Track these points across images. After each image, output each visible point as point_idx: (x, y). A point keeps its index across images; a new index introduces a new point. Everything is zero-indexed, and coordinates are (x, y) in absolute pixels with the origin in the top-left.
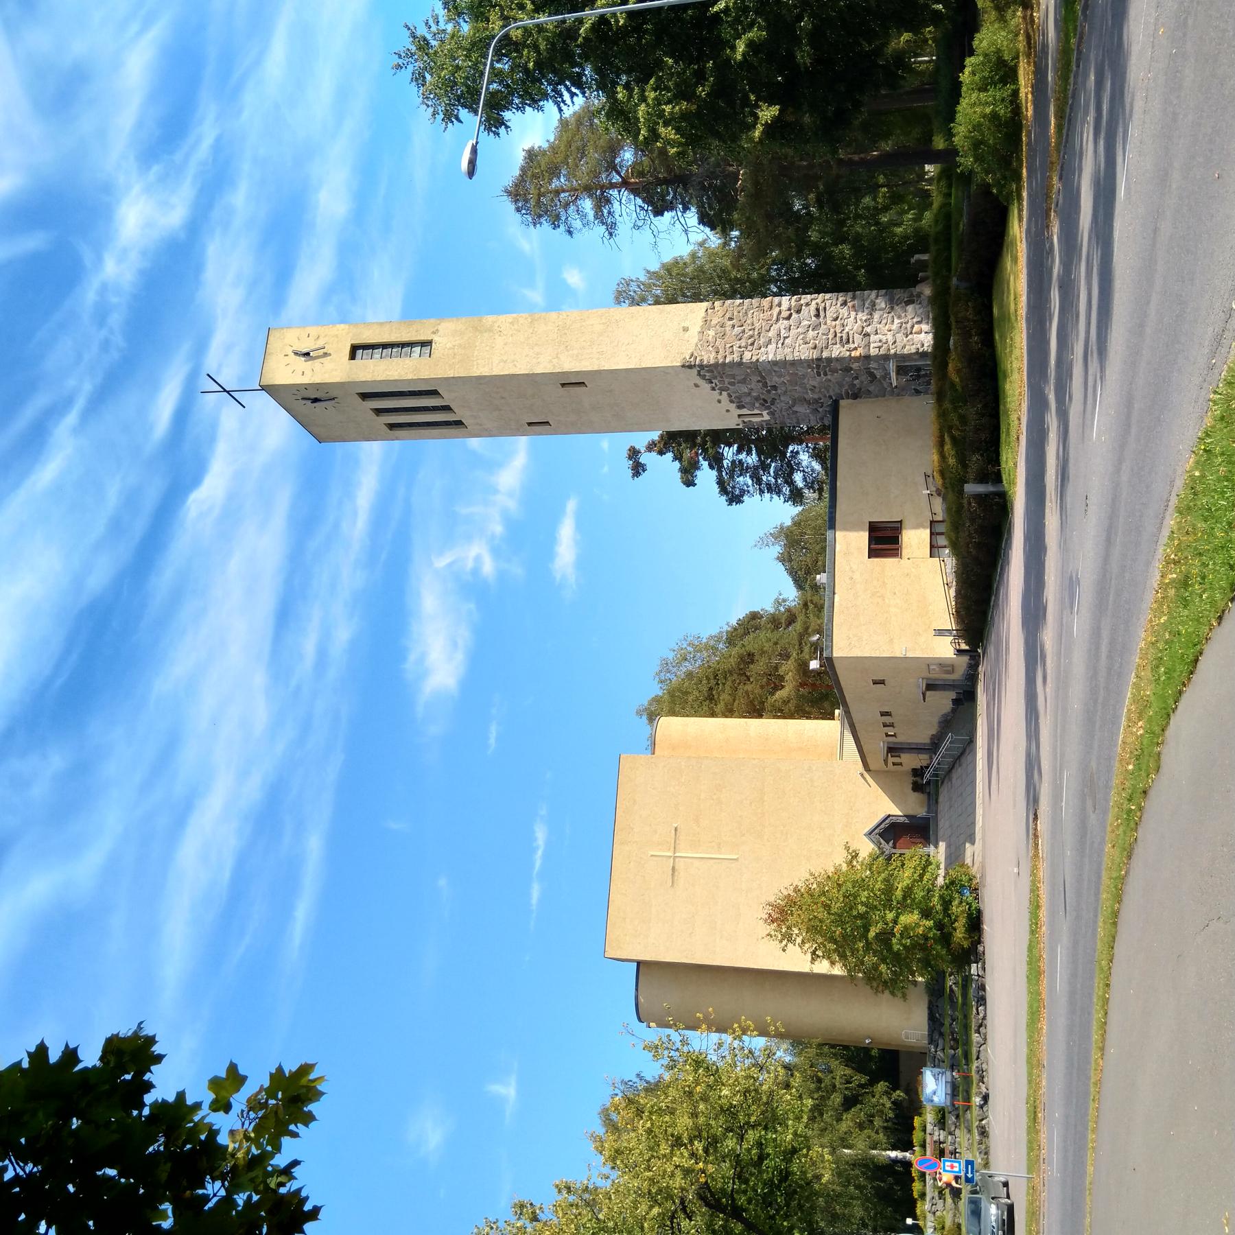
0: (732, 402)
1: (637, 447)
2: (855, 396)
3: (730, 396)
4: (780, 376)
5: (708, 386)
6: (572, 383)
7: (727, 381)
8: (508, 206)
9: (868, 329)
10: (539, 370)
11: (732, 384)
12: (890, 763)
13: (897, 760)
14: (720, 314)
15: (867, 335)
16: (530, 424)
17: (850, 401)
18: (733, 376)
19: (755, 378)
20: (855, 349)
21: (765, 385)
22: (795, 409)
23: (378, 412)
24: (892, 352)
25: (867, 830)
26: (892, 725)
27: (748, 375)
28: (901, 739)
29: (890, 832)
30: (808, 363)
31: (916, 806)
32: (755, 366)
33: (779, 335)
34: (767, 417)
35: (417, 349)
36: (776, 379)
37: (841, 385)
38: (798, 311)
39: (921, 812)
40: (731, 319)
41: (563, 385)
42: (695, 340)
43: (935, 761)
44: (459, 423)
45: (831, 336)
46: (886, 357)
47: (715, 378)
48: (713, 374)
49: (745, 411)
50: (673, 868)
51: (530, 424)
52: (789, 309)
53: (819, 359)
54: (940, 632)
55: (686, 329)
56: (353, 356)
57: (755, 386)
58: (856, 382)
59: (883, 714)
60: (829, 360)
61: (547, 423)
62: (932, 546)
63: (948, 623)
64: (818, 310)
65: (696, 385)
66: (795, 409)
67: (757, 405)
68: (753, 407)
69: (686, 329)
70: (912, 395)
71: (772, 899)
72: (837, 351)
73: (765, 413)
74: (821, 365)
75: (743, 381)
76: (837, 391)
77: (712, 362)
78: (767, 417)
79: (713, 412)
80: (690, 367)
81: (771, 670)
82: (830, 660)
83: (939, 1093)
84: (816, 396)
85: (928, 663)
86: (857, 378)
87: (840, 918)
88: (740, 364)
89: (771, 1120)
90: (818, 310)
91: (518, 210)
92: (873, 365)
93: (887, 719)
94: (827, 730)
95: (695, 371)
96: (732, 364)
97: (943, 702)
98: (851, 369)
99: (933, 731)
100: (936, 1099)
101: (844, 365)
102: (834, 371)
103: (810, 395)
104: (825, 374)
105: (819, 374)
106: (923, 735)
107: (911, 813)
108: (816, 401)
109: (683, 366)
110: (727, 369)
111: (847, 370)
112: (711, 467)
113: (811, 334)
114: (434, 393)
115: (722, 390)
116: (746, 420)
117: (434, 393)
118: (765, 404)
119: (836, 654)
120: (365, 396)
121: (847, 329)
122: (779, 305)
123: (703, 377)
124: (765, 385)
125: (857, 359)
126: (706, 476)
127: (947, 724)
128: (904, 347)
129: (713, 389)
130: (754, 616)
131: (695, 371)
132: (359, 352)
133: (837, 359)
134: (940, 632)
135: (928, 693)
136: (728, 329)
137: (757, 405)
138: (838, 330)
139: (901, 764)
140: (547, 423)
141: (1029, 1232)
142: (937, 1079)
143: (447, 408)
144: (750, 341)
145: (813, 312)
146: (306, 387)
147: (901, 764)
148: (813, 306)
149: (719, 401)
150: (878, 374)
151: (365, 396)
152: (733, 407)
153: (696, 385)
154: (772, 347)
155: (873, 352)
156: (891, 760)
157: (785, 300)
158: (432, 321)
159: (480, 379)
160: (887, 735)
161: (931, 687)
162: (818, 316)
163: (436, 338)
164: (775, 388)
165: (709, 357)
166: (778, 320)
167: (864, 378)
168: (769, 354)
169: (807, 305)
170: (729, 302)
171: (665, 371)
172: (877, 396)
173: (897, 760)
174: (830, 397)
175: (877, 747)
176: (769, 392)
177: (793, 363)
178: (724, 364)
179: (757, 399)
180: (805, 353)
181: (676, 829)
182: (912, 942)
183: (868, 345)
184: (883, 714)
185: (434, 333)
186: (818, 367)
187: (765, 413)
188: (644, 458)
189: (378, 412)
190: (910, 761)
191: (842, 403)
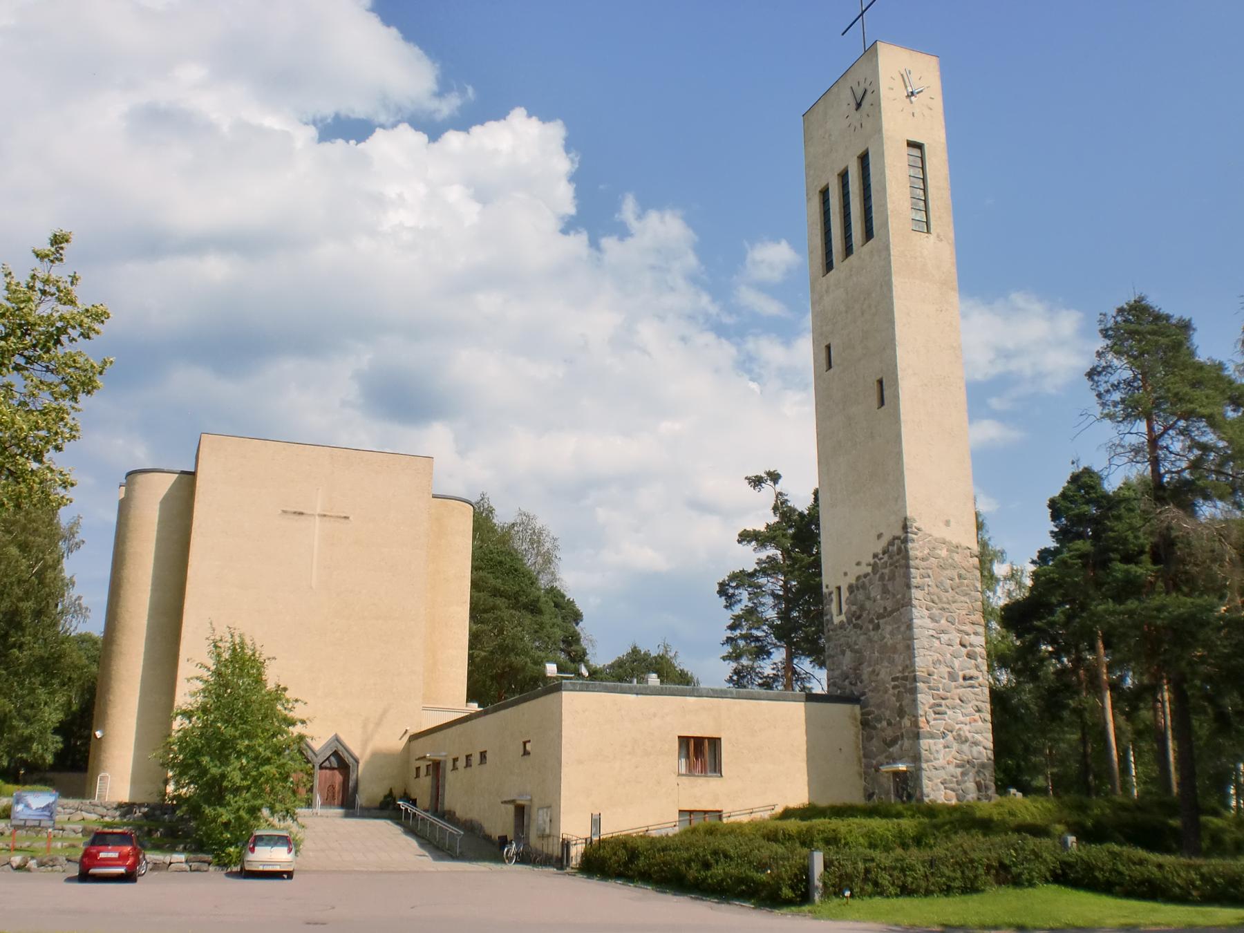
0: (858, 578)
1: (780, 481)
2: (865, 724)
3: (866, 576)
4: (892, 633)
5: (879, 550)
6: (883, 391)
7: (886, 571)
8: (1125, 298)
9: (950, 737)
10: (900, 352)
11: (882, 578)
12: (418, 764)
13: (423, 771)
14: (965, 564)
15: (944, 735)
16: (828, 347)
17: (859, 717)
18: (892, 578)
19: (889, 604)
20: (928, 722)
21: (880, 616)
22: (848, 653)
23: (844, 176)
24: (924, 766)
25: (343, 737)
26: (468, 765)
27: (894, 596)
28: (450, 776)
29: (340, 761)
30: (910, 666)
31: (370, 792)
32: (907, 603)
33: (943, 632)
34: (837, 620)
35: (921, 216)
36: (889, 628)
37: (879, 706)
38: (969, 656)
39: (361, 800)
40: (960, 576)
41: (880, 382)
42: (936, 534)
43: (421, 813)
44: (829, 266)
45: (941, 692)
46: (916, 758)
47: (891, 557)
48: (895, 559)
49: (845, 594)
50: (301, 514)
51: (828, 347)
52: (971, 645)
53: (915, 679)
54: (596, 822)
55: (947, 523)
56: (911, 144)
57: (880, 602)
58: (884, 723)
59: (483, 755)
60: (914, 691)
61: (830, 366)
62: (691, 812)
63: (609, 829)
64: (971, 678)
65: (880, 536)
66: (848, 653)
67: (854, 608)
68: (851, 602)
69: (947, 523)
70: (865, 789)
71: (248, 641)
72: (924, 699)
73: (843, 618)
74: (907, 683)
75: (885, 591)
76: (872, 702)
77: (911, 553)
78: (837, 620)
79: (842, 561)
80: (905, 528)
81: (520, 634)
82: (558, 688)
83: (29, 812)
84: (865, 677)
85: (552, 807)
86: (889, 724)
87: (242, 701)
88: (908, 586)
89: (10, 732)
90: (971, 678)
91: (1121, 311)
92: (907, 743)
93: (476, 759)
94: (454, 699)
95: (899, 533)
96: (907, 576)
97: (499, 823)
98: (902, 717)
99: (460, 813)
100: (20, 807)
101: (906, 707)
102: (899, 697)
103: (866, 670)
104: (894, 687)
105: (893, 679)
106: (454, 799)
107: (361, 788)
108: (858, 677)
109: (906, 519)
110: (902, 571)
111: (901, 713)
112: (759, 562)
113: (944, 670)
114: (869, 234)
115: (874, 566)
116: (834, 596)
117: (869, 234)
118: (855, 618)
119: (564, 693)
120: (864, 159)
121: (949, 712)
122: (976, 634)
123: (891, 543)
124: (880, 616)
125: (915, 724)
126: (749, 558)
127: (471, 828)
128: (930, 779)
129: (875, 556)
130: (577, 617)
131: (899, 533)
132: (916, 152)
133: (915, 700)
134: (596, 822)
135: (511, 808)
136: (949, 573)
137: (854, 608)
138: (948, 702)
139: (418, 776)
140: (830, 366)
141: (1240, 848)
142: (44, 809)
143: (848, 250)
144: (935, 598)
145: (969, 672)
146: (876, 92)
147: (418, 776)
148: (974, 672)
149: (858, 564)
150: (894, 750)
151: (864, 159)
152: (851, 579)
153: (880, 536)
154: (928, 622)
155: (924, 743)
156: (423, 765)
157: (981, 640)
158: (952, 235)
159: (887, 285)
160: (455, 760)
161: (520, 811)
162: (965, 678)
163: (932, 237)
164: (877, 627)
165: (916, 549)
166: (959, 631)
167: (889, 733)
168: (921, 619)
169: (977, 667)
170: (978, 573)
171: (900, 496)
172: (864, 748)
173: (423, 771)
174: (864, 694)
175: (430, 751)
176: (871, 621)
177: (910, 649)
178: (908, 567)
179: (862, 608)
180: (922, 662)
181: (346, 518)
182: (229, 780)
183: (932, 736)
184: (483, 755)
185: (938, 236)
186: (905, 678)
187: (843, 618)
188: (768, 487)
189: (844, 176)
190: (422, 788)
191: (857, 708)
